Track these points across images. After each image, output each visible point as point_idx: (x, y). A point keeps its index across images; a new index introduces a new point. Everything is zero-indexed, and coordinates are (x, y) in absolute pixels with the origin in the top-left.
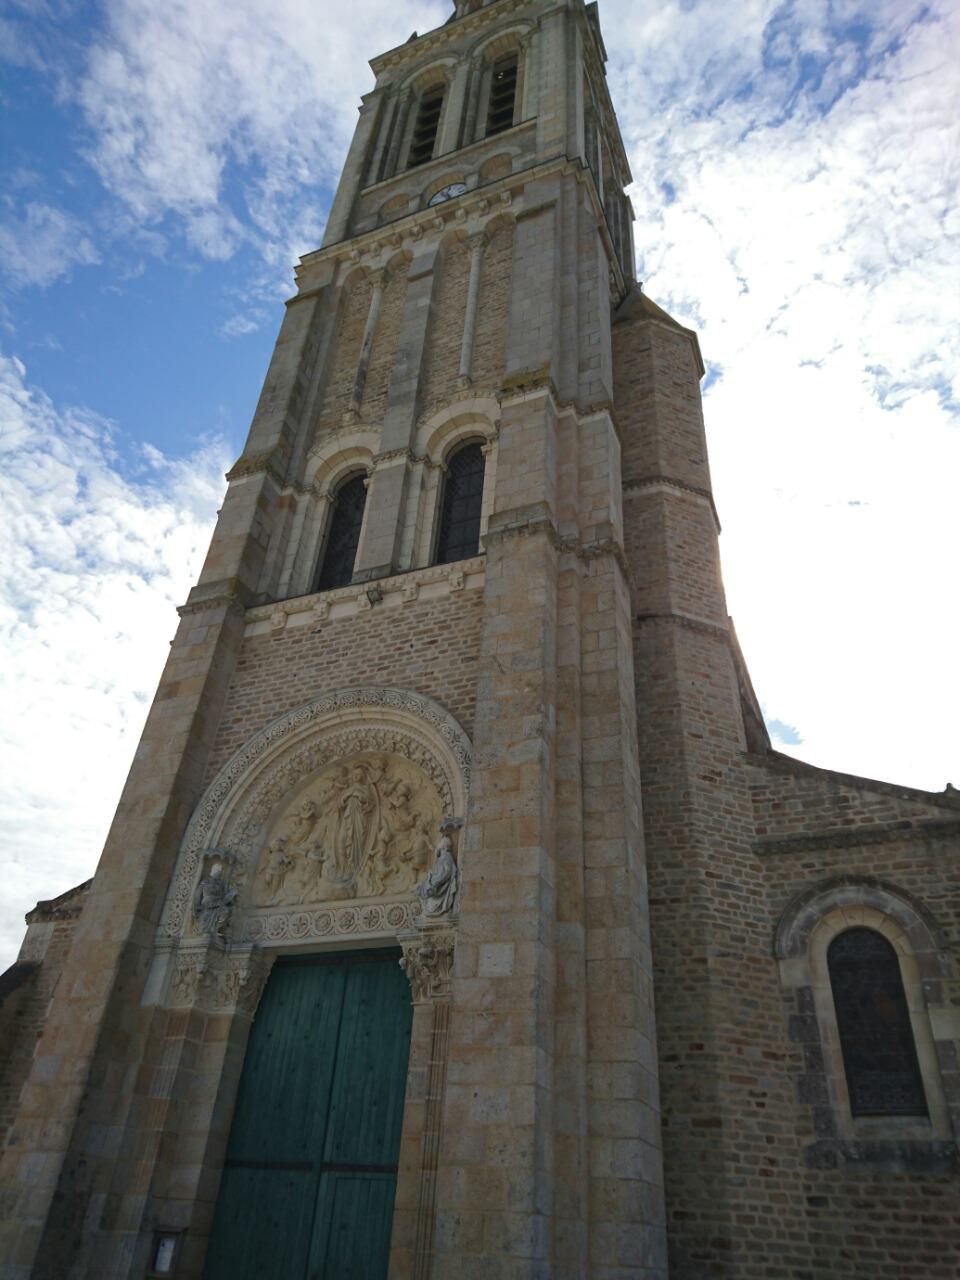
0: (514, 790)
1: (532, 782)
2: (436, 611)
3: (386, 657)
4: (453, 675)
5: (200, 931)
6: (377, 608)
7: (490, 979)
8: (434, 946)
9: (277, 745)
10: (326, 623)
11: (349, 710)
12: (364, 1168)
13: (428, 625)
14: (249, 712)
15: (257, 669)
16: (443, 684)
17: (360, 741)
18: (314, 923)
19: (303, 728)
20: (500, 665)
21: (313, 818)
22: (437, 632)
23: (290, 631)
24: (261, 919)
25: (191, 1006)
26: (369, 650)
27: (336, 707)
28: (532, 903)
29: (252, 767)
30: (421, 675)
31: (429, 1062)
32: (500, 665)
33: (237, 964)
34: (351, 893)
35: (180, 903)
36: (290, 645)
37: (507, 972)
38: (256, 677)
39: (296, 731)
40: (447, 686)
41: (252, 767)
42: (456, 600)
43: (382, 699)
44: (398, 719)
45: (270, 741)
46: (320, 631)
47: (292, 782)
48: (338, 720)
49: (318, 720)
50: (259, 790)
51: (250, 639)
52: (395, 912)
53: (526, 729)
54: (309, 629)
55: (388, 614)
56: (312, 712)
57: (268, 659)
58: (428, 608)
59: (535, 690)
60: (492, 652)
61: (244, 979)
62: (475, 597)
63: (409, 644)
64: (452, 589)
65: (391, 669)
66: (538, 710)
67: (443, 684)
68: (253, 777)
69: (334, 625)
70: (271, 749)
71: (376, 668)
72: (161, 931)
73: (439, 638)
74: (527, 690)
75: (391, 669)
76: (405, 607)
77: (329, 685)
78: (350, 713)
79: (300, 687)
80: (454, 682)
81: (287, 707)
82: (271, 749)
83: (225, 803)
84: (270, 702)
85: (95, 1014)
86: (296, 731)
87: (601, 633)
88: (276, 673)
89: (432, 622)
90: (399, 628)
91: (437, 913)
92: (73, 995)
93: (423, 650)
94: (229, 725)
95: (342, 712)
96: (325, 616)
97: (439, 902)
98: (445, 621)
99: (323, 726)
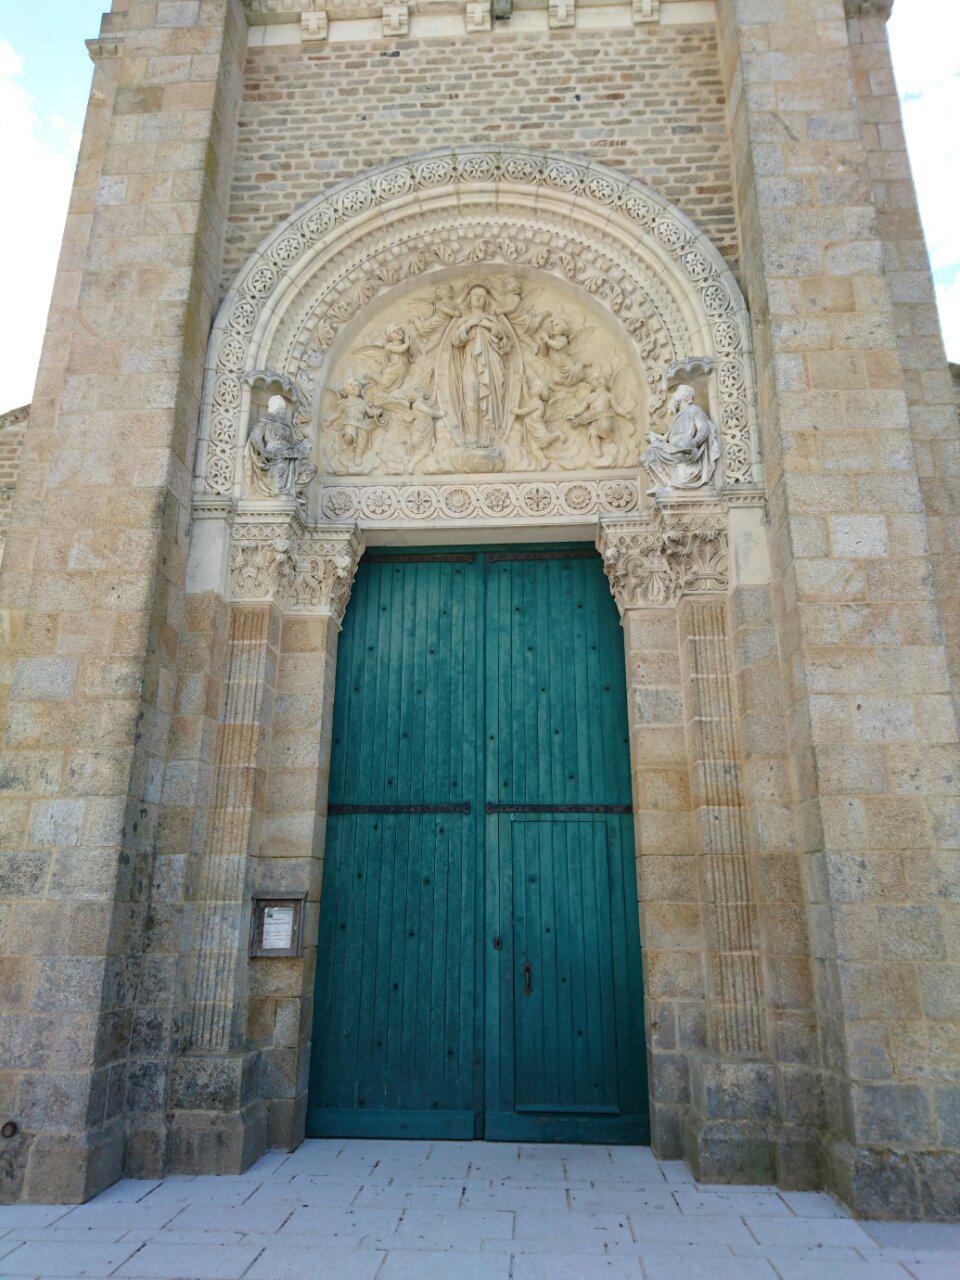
0: (847, 311)
1: (875, 301)
2: (611, 50)
3: (532, 110)
4: (663, 151)
5: (277, 491)
6: (500, 30)
7: (854, 560)
8: (686, 529)
9: (349, 225)
10: (405, 43)
11: (478, 185)
12: (552, 809)
13: (601, 69)
14: (286, 166)
15: (285, 100)
16: (646, 162)
17: (486, 243)
18: (443, 500)
19: (394, 203)
20: (786, 128)
21: (409, 354)
22: (618, 81)
23: (339, 47)
24: (348, 491)
25: (269, 598)
26: (499, 94)
27: (455, 175)
28: (904, 465)
29: (310, 253)
30: (603, 143)
31: (693, 675)
32: (786, 128)
33: (328, 547)
34: (495, 464)
35: (227, 447)
36: (342, 69)
37: (880, 551)
38: (287, 112)
39: (384, 207)
40: (653, 165)
41: (310, 253)
42: (648, 37)
43: (541, 172)
44: (564, 210)
45: (341, 216)
46: (396, 54)
47: (369, 293)
48: (453, 201)
49: (422, 194)
50: (318, 296)
51: (261, 51)
52: (576, 493)
53: (852, 225)
54: (374, 48)
55: (520, 42)
56: (413, 177)
57: (305, 86)
58: (597, 44)
59: (856, 171)
60: (769, 107)
61: (344, 569)
62: (680, 38)
63: (572, 94)
64: (638, 18)
65: (546, 128)
66: (867, 200)
67: (646, 162)
68: (319, 264)
69: (423, 47)
70: (341, 229)
71: (518, 124)
72: (200, 485)
73: (627, 93)
74: (840, 168)
75: (546, 128)
76: (553, 37)
77: (433, 140)
78: (476, 190)
79: (377, 137)
80: (665, 161)
81: (361, 167)
82: (341, 229)
83: (270, 303)
84: (324, 154)
85: (134, 594)
86: (384, 207)
87: (880, 127)
88: (324, 111)
89: (610, 65)
90: (549, 67)
91: (696, 485)
92: (72, 565)
93: (600, 106)
94: (252, 182)
95: (464, 186)
96: (404, 30)
97: (695, 470)
98: (632, 67)
99: (426, 207)
